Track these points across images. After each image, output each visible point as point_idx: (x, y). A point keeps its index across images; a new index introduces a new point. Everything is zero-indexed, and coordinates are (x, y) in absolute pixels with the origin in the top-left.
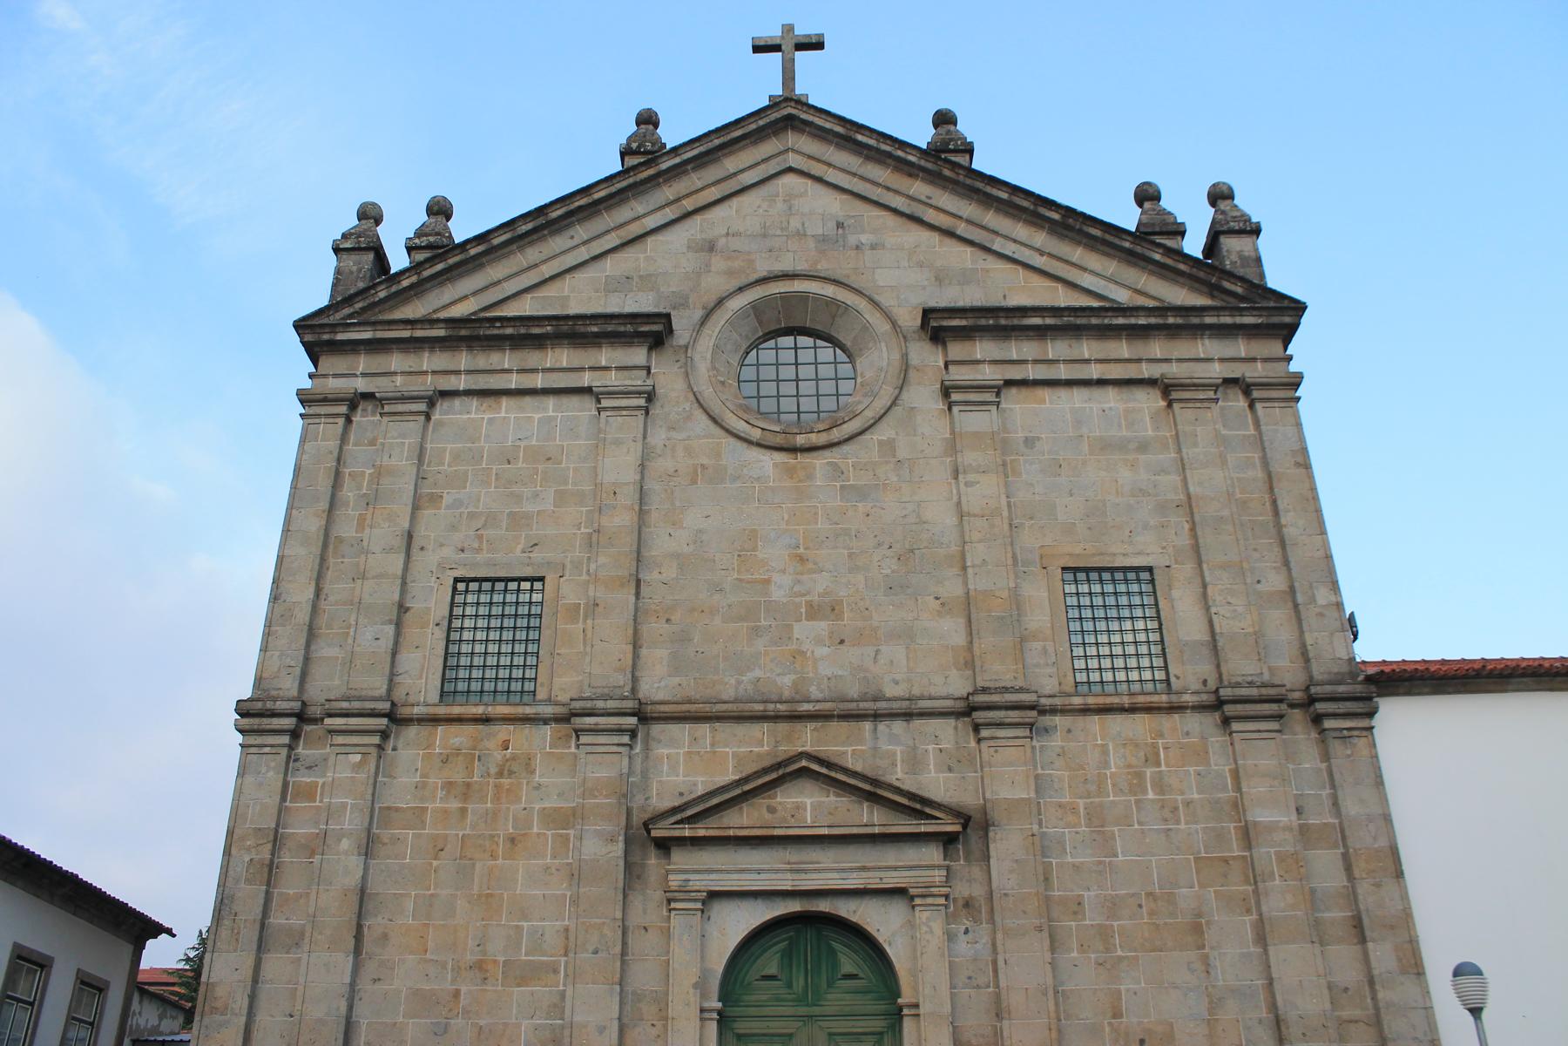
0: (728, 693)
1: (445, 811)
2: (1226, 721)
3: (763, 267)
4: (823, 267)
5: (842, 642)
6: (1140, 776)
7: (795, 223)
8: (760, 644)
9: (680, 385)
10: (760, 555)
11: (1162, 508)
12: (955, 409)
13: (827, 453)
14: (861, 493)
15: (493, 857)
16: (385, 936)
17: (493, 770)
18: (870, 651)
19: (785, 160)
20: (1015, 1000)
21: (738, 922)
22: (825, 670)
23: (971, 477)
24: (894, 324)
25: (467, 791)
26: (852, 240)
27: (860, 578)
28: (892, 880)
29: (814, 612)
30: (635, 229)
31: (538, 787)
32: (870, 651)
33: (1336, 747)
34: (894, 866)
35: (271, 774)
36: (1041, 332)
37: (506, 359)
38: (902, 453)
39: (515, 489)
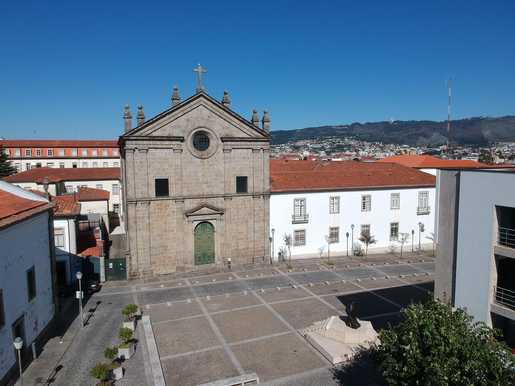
0: (194, 195)
1: (158, 212)
2: (253, 198)
3: (197, 125)
4: (206, 125)
5: (209, 187)
6: (243, 204)
7: (202, 116)
8: (198, 188)
9: (185, 147)
10: (198, 175)
11: (250, 168)
12: (225, 153)
13: (207, 159)
14: (211, 165)
15: (166, 217)
16: (153, 228)
17: (164, 206)
18: (212, 188)
19: (200, 103)
20: (227, 230)
24: (217, 137)
25: (161, 209)
26: (211, 120)
28: (214, 218)
29: (205, 183)
30: (176, 117)
32: (212, 188)
33: (265, 200)
34: (214, 216)
35: (133, 209)
36: (237, 141)
37: (158, 142)
38: (217, 159)
39: (162, 164)
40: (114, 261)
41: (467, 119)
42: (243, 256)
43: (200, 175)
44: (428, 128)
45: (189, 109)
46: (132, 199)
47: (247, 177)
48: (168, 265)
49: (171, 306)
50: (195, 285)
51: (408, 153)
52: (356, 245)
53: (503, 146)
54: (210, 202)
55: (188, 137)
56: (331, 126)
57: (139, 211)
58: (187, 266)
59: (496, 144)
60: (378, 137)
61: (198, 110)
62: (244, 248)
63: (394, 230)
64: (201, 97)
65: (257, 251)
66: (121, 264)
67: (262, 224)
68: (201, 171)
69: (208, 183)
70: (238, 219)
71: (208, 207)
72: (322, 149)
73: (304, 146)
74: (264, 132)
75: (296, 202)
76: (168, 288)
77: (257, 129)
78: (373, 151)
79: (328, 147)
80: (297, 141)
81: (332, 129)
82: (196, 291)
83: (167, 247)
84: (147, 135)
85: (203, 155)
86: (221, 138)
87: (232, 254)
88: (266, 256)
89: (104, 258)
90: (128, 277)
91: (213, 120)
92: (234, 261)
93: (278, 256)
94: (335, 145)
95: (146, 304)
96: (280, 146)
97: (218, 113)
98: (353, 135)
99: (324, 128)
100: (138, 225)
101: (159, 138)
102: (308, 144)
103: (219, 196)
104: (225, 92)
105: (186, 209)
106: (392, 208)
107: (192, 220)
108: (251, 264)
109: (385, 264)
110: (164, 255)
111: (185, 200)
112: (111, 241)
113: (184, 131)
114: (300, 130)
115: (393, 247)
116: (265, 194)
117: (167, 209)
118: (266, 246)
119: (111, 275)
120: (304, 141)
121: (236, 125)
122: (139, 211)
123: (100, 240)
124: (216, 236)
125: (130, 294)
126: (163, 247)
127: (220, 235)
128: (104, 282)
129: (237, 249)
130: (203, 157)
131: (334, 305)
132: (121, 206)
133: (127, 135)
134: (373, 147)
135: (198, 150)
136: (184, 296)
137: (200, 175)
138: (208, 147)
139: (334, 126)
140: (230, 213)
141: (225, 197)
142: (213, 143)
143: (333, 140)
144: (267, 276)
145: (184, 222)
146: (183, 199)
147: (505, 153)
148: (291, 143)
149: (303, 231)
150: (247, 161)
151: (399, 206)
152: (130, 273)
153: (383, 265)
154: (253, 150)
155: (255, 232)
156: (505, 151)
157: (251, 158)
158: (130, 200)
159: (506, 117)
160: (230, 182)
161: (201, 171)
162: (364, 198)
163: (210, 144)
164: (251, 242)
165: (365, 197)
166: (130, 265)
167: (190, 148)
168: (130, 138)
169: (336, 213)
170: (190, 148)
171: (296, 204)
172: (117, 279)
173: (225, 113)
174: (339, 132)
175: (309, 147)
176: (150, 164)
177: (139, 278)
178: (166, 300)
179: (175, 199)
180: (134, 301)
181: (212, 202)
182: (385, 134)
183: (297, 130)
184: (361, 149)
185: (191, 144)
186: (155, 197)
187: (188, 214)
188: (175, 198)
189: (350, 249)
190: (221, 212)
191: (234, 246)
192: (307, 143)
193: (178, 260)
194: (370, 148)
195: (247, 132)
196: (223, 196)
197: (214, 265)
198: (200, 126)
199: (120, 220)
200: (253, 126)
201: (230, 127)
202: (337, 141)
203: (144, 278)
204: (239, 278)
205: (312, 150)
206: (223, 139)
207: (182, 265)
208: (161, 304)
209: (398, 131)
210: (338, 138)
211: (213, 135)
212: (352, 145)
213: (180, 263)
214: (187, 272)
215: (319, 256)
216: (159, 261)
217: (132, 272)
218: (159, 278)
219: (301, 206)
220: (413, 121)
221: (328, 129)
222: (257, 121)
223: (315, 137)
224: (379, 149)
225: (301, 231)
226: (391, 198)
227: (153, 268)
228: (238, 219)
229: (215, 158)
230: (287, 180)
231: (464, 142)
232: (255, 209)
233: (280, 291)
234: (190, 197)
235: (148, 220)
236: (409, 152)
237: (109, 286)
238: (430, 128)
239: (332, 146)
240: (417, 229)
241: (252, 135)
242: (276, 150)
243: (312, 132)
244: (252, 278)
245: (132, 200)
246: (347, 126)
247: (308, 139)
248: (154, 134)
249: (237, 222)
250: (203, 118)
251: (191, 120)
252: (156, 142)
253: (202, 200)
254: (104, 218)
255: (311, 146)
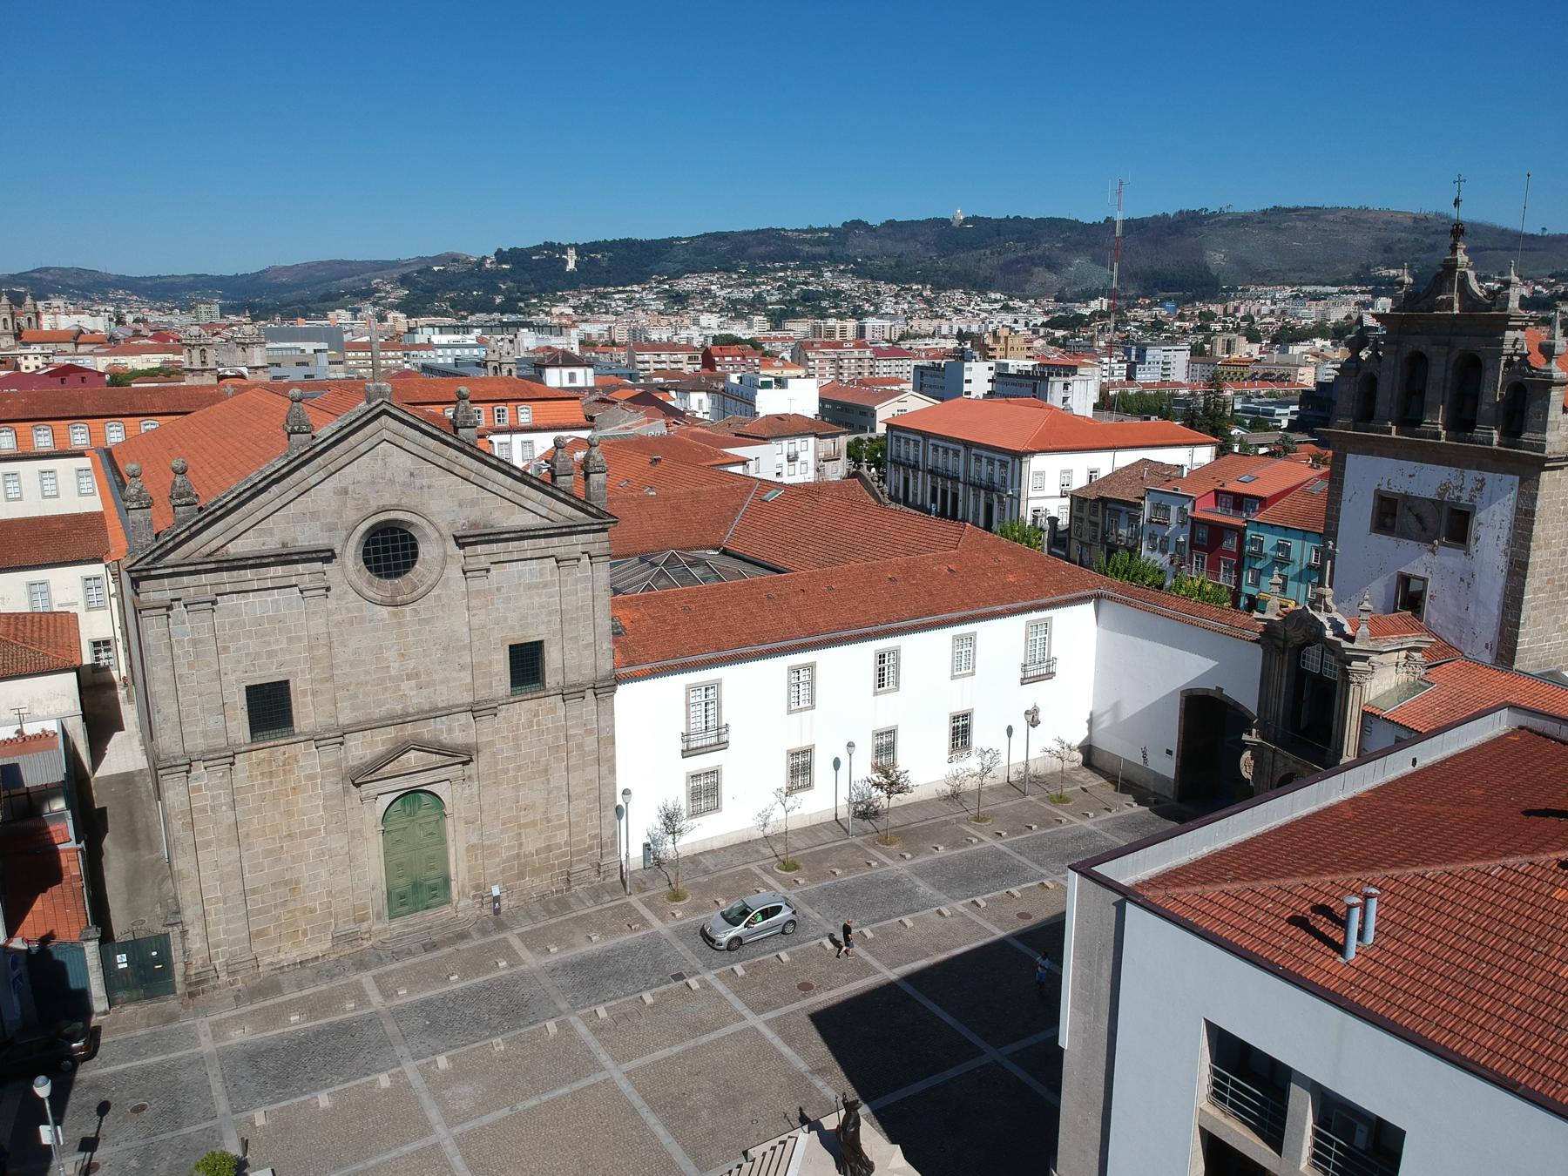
0: (377, 716)
1: (263, 784)
3: (374, 505)
6: (532, 721)
7: (388, 475)
11: (550, 614)
14: (427, 621)
15: (287, 796)
18: (432, 689)
20: (485, 807)
21: (386, 800)
22: (415, 701)
23: (474, 612)
24: (441, 535)
27: (428, 659)
28: (443, 777)
29: (409, 678)
30: (304, 485)
31: (302, 767)
32: (432, 689)
37: (249, 573)
38: (445, 601)
40: (131, 947)
41: (1165, 216)
42: (536, 872)
43: (391, 654)
44: (1058, 242)
45: (345, 459)
46: (175, 758)
47: (542, 642)
48: (305, 933)
49: (331, 1106)
50: (398, 1002)
51: (1002, 341)
52: (858, 788)
53: (1258, 298)
54: (426, 731)
55: (344, 546)
56: (783, 229)
57: (200, 790)
58: (364, 926)
59: (1242, 290)
60: (920, 266)
61: (375, 458)
62: (540, 849)
63: (961, 732)
64: (384, 418)
65: (579, 853)
66: (154, 953)
67: (591, 772)
68: (393, 645)
69: (417, 675)
70: (519, 768)
71: (422, 747)
72: (757, 304)
73: (701, 293)
74: (592, 506)
75: (692, 694)
76: (313, 1023)
77: (569, 499)
78: (905, 312)
79: (774, 299)
80: (677, 275)
81: (785, 239)
82: (401, 1030)
83: (297, 882)
84: (208, 555)
85: (398, 591)
86: (456, 538)
87: (503, 872)
88: (606, 860)
89: (97, 943)
90: (180, 988)
91: (425, 482)
92: (509, 890)
93: (640, 853)
94: (795, 291)
95: (252, 1106)
96: (626, 292)
97: (441, 462)
98: (847, 260)
99: (761, 236)
100: (201, 832)
101: (251, 562)
102: (713, 287)
103: (455, 710)
104: (460, 392)
105: (351, 763)
106: (956, 673)
107: (373, 792)
108: (562, 890)
109: (937, 848)
110: (291, 906)
111: (346, 736)
112: (103, 810)
113: (331, 528)
114: (685, 239)
115: (956, 778)
116: (601, 685)
117: (291, 771)
118: (606, 834)
119: (126, 987)
120: (701, 278)
121: (502, 491)
122: (199, 789)
123: (72, 845)
124: (450, 829)
125: (196, 1062)
126: (286, 883)
127: (463, 824)
128: (105, 1013)
129: (518, 855)
130: (399, 598)
131: (802, 1052)
132: (120, 645)
133: (142, 563)
134: (904, 299)
135: (380, 576)
136: (369, 1057)
137: (391, 654)
138: (414, 563)
139: (791, 231)
140: (494, 755)
141: (475, 710)
142: (427, 551)
143: (789, 273)
144: (611, 943)
145: (348, 800)
146: (341, 735)
147: (1263, 321)
148: (660, 282)
149: (713, 772)
150: (540, 595)
151: (974, 667)
152: (186, 976)
153: (932, 853)
154: (557, 562)
155: (572, 799)
156: (1265, 316)
157: (554, 585)
158: (169, 764)
159: (1271, 210)
160: (490, 664)
161: (393, 645)
162: (881, 658)
163: (421, 556)
164: (561, 827)
165: (884, 656)
166: (184, 952)
167: (353, 577)
168: (153, 573)
169: (806, 709)
170: (353, 577)
171: (693, 700)
172: (146, 998)
173: (465, 459)
174: (806, 248)
175: (715, 297)
176: (224, 641)
177: (214, 988)
178: (315, 1083)
179: (317, 739)
180: (214, 1094)
181: (435, 729)
182: (939, 257)
183: (679, 239)
184: (872, 305)
185: (356, 564)
186: (248, 740)
187: (359, 777)
188: (316, 738)
189: (843, 802)
190: (463, 756)
191: (510, 848)
192: (712, 283)
193: (337, 915)
194: (896, 303)
195: (537, 509)
196: (469, 708)
197: (448, 910)
198: (384, 506)
199: (122, 693)
200: (555, 492)
201: (483, 498)
202: (801, 279)
203: (231, 985)
204: (531, 961)
205: (727, 307)
206: (460, 541)
207: (350, 927)
208: (298, 1100)
209: (976, 249)
210: (805, 269)
211: (429, 530)
212: (843, 292)
213: (345, 922)
214: (367, 944)
215: (761, 835)
216: (276, 928)
217: (192, 973)
218: (281, 977)
219: (706, 704)
220: (1017, 218)
221: (774, 237)
222: (569, 472)
223: (734, 262)
224: (922, 306)
225: (707, 773)
226: (953, 647)
227: (258, 948)
228: (519, 768)
229: (439, 597)
230: (665, 621)
231: (1156, 285)
232: (571, 732)
233: (652, 1007)
234: (363, 727)
235: (230, 813)
236: (1006, 338)
237: (125, 1029)
238: (1064, 240)
239: (785, 294)
240: (1020, 725)
241: (552, 515)
242: (613, 304)
243: (724, 247)
244: (569, 955)
245: (174, 763)
246: (829, 230)
247: (714, 271)
248: (235, 549)
249: (515, 778)
250: (392, 481)
251: (354, 491)
252: (242, 572)
253: (402, 730)
254: (69, 729)
255: (722, 293)
